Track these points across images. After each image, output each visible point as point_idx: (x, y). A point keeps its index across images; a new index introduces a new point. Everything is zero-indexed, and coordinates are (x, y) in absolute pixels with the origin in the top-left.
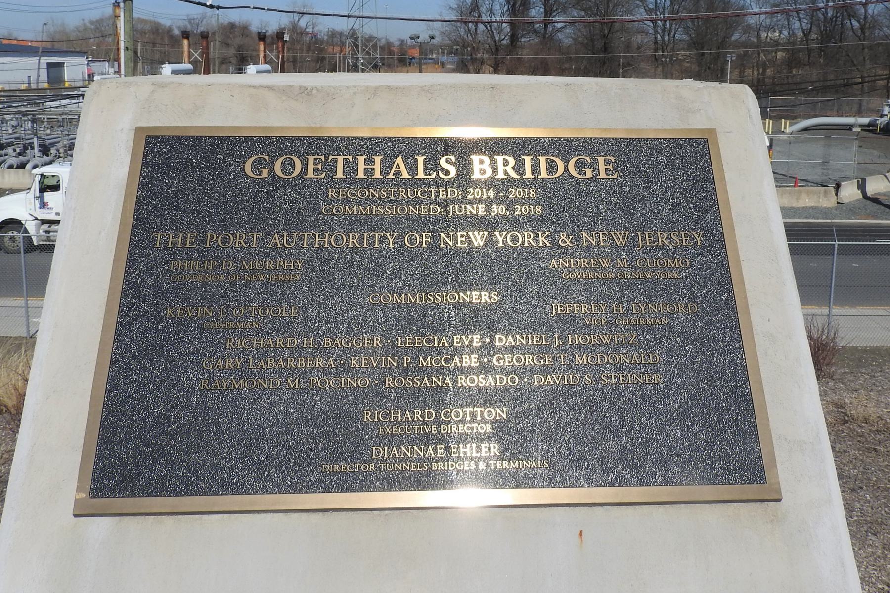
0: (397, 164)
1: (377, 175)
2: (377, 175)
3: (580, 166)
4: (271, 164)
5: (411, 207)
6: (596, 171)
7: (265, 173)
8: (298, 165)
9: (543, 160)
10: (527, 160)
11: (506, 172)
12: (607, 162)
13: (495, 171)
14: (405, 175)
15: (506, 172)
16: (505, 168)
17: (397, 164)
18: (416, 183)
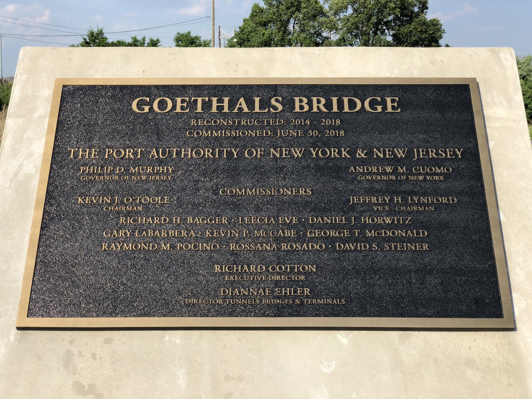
0: (241, 103)
1: (226, 110)
2: (226, 110)
3: (372, 104)
4: (151, 104)
5: (250, 131)
6: (385, 108)
7: (146, 109)
8: (134, 247)
9: (346, 100)
10: (335, 100)
11: (318, 108)
12: (393, 101)
13: (311, 107)
14: (246, 110)
15: (318, 108)
16: (318, 105)
17: (241, 103)
18: (251, 115)
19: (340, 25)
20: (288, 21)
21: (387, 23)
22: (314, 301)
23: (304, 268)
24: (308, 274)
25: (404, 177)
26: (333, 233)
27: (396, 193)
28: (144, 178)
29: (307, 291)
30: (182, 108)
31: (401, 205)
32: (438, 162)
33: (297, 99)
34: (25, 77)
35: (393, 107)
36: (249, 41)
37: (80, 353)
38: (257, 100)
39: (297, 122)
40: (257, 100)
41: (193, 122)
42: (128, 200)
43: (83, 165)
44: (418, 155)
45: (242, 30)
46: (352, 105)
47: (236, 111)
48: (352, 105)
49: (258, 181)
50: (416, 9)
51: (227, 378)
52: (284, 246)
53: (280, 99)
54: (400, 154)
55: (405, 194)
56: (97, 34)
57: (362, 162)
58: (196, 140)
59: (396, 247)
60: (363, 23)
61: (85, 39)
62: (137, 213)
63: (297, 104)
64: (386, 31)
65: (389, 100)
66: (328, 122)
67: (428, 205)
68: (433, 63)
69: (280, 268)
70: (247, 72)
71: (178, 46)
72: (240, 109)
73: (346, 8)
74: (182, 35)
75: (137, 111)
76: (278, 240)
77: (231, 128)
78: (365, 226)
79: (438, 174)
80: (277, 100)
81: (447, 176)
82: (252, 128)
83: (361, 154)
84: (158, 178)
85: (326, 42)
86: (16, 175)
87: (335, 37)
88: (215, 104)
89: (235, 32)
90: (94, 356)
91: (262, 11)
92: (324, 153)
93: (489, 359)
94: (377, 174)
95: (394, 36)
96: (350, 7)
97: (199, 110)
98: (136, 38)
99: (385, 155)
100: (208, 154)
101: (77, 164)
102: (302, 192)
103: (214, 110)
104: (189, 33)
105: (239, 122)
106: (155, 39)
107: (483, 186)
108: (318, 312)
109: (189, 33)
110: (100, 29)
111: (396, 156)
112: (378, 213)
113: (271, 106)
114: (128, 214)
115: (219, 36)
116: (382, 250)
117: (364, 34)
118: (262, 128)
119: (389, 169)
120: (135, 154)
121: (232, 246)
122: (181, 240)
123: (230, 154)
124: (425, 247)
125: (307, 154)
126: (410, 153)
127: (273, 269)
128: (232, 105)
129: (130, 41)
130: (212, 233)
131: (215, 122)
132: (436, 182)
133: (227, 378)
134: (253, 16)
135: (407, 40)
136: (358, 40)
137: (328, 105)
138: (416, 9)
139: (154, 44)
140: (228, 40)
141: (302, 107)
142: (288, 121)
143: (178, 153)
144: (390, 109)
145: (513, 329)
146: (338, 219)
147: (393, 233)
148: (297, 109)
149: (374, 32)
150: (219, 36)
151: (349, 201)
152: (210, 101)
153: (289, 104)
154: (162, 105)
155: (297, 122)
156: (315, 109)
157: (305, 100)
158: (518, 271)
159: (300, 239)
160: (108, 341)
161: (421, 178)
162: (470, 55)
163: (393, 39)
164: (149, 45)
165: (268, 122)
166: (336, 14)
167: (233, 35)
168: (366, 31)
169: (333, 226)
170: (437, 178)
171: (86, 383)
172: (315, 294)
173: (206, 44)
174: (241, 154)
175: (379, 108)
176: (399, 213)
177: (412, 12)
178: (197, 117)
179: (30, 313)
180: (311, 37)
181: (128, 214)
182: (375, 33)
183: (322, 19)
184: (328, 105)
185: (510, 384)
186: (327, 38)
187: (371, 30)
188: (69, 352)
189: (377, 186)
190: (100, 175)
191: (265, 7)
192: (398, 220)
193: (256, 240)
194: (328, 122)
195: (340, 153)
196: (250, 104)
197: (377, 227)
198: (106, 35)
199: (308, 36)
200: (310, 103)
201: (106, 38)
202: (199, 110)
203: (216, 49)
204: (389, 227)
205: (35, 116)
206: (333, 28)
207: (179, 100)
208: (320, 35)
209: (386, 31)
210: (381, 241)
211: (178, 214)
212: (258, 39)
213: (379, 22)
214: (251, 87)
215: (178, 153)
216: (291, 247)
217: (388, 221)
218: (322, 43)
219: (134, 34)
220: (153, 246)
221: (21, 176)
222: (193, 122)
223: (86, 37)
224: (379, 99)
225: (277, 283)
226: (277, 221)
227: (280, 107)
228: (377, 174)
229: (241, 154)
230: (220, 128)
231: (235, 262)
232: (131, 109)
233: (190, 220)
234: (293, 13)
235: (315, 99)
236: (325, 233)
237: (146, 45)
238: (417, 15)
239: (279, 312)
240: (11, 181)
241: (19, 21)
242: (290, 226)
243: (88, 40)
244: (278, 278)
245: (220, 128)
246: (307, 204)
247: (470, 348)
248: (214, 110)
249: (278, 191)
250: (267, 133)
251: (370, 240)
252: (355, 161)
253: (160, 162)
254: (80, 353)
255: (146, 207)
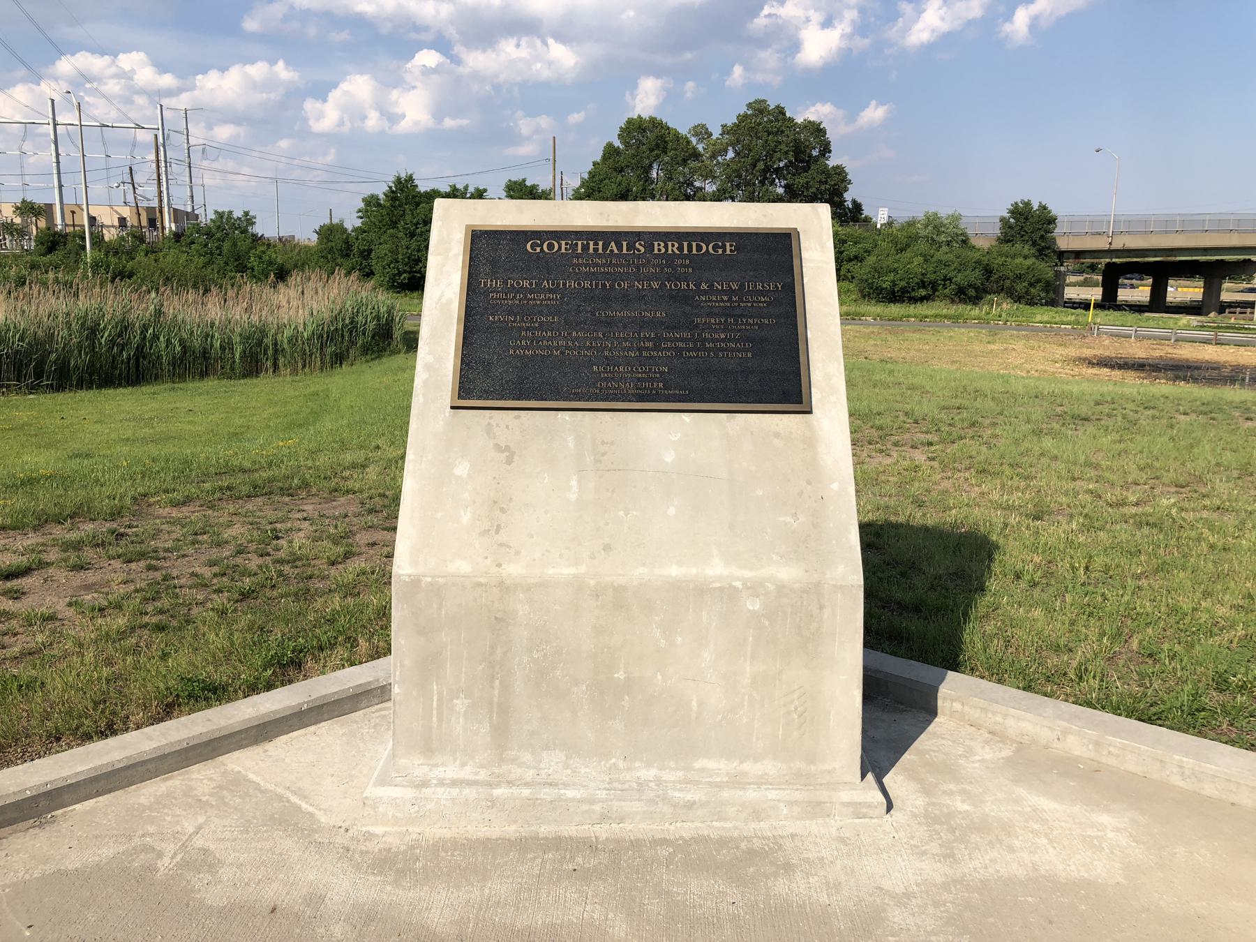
1: (600, 251)
2: (600, 251)
4: (541, 245)
6: (724, 251)
7: (538, 249)
9: (694, 244)
10: (685, 244)
12: (731, 246)
13: (667, 250)
14: (616, 251)
19: (718, 172)
20: (650, 167)
21: (778, 170)
22: (666, 392)
23: (659, 369)
24: (662, 373)
25: (736, 304)
26: (681, 345)
27: (730, 316)
28: (538, 302)
29: (661, 385)
30: (566, 249)
31: (733, 324)
32: (762, 293)
33: (656, 244)
34: (440, 223)
35: (731, 251)
36: (600, 192)
37: (497, 425)
38: (625, 244)
39: (655, 261)
40: (625, 244)
41: (575, 261)
42: (527, 319)
43: (491, 292)
44: (749, 287)
45: (592, 175)
46: (699, 248)
47: (608, 252)
48: (699, 248)
49: (625, 306)
50: (815, 153)
51: (603, 443)
52: (644, 354)
53: (643, 243)
54: (735, 287)
55: (736, 316)
56: (406, 180)
57: (705, 292)
58: (577, 274)
59: (727, 355)
60: (747, 170)
61: (390, 187)
62: (535, 329)
63: (656, 247)
64: (777, 181)
65: (728, 244)
66: (680, 262)
67: (753, 325)
68: (765, 216)
69: (642, 369)
70: (617, 221)
71: (512, 197)
72: (612, 251)
73: (726, 151)
74: (515, 183)
75: (531, 251)
76: (640, 349)
77: (604, 265)
78: (705, 340)
79: (762, 302)
80: (640, 244)
81: (769, 304)
82: (621, 266)
83: (704, 286)
84: (549, 302)
85: (699, 194)
86: (440, 300)
87: (710, 188)
88: (591, 247)
89: (582, 178)
90: (507, 427)
91: (617, 151)
92: (676, 285)
93: (791, 432)
94: (715, 302)
95: (786, 187)
96: (730, 148)
97: (579, 251)
98: (455, 186)
99: (722, 287)
100: (587, 285)
101: (487, 292)
102: (658, 315)
103: (591, 251)
104: (524, 180)
105: (611, 261)
106: (481, 188)
107: (795, 311)
108: (667, 399)
109: (524, 180)
110: (409, 173)
111: (731, 288)
112: (716, 331)
113: (635, 249)
114: (528, 329)
115: (562, 184)
116: (717, 357)
117: (748, 184)
118: (629, 265)
119: (725, 298)
120: (531, 284)
121: (606, 353)
122: (567, 347)
123: (604, 285)
124: (749, 355)
125: (662, 286)
126: (742, 286)
127: (636, 369)
128: (605, 248)
129: (448, 189)
130: (591, 344)
131: (592, 261)
132: (760, 307)
133: (603, 443)
134: (604, 158)
135: (803, 192)
136: (740, 192)
137: (681, 248)
138: (815, 153)
139: (480, 194)
140: (574, 190)
141: (659, 250)
142: (649, 261)
143: (564, 284)
144: (728, 252)
145: (810, 412)
146: (686, 335)
147: (726, 345)
148: (656, 251)
149: (760, 182)
150: (562, 184)
151: (694, 321)
152: (588, 244)
153: (650, 248)
154: (551, 246)
155: (655, 261)
156: (670, 252)
157: (662, 244)
158: (817, 373)
159: (656, 348)
160: (518, 417)
161: (750, 305)
162: (795, 210)
163: (785, 191)
164: (472, 197)
165: (633, 261)
166: (713, 156)
167: (579, 183)
168: (750, 180)
169: (682, 340)
170: (761, 305)
171: (503, 445)
172: (665, 387)
173: (545, 196)
174: (612, 286)
175: (720, 251)
176: (731, 330)
177: (810, 156)
178: (578, 257)
179: (460, 397)
180: (680, 187)
181: (528, 329)
182: (762, 183)
183: (693, 164)
184: (681, 248)
185: (804, 449)
186: (701, 189)
187: (757, 179)
188: (489, 424)
189: (716, 311)
190: (504, 299)
191: (621, 147)
192: (731, 336)
193: (624, 349)
194: (680, 262)
195: (688, 285)
196: (620, 247)
197: (714, 341)
198: (416, 182)
199: (677, 187)
200: (666, 247)
201: (417, 186)
202: (579, 251)
203: (558, 202)
204: (723, 340)
205: (451, 254)
206: (709, 175)
207: (563, 243)
208: (692, 184)
209: (777, 181)
210: (716, 350)
211: (565, 330)
212: (614, 189)
213: (767, 170)
214: (620, 233)
215: (564, 284)
216: (650, 354)
217: (723, 336)
218: (694, 195)
219: (452, 181)
220: (547, 352)
221: (444, 300)
222: (575, 261)
223: (391, 184)
224: (720, 244)
225: (639, 380)
226: (639, 335)
227: (643, 250)
228: (715, 302)
229: (612, 286)
230: (597, 265)
231: (608, 365)
232: (526, 250)
233: (574, 334)
234: (658, 156)
235: (670, 244)
236: (675, 345)
237: (468, 195)
238: (816, 159)
239: (641, 399)
240: (437, 304)
241: (296, 162)
242: (649, 339)
243: (394, 189)
244: (640, 375)
245: (597, 265)
246: (662, 323)
247: (777, 425)
248: (591, 251)
249: (641, 313)
250: (632, 270)
251: (709, 350)
252: (700, 292)
253: (550, 291)
254: (497, 425)
255: (541, 324)
